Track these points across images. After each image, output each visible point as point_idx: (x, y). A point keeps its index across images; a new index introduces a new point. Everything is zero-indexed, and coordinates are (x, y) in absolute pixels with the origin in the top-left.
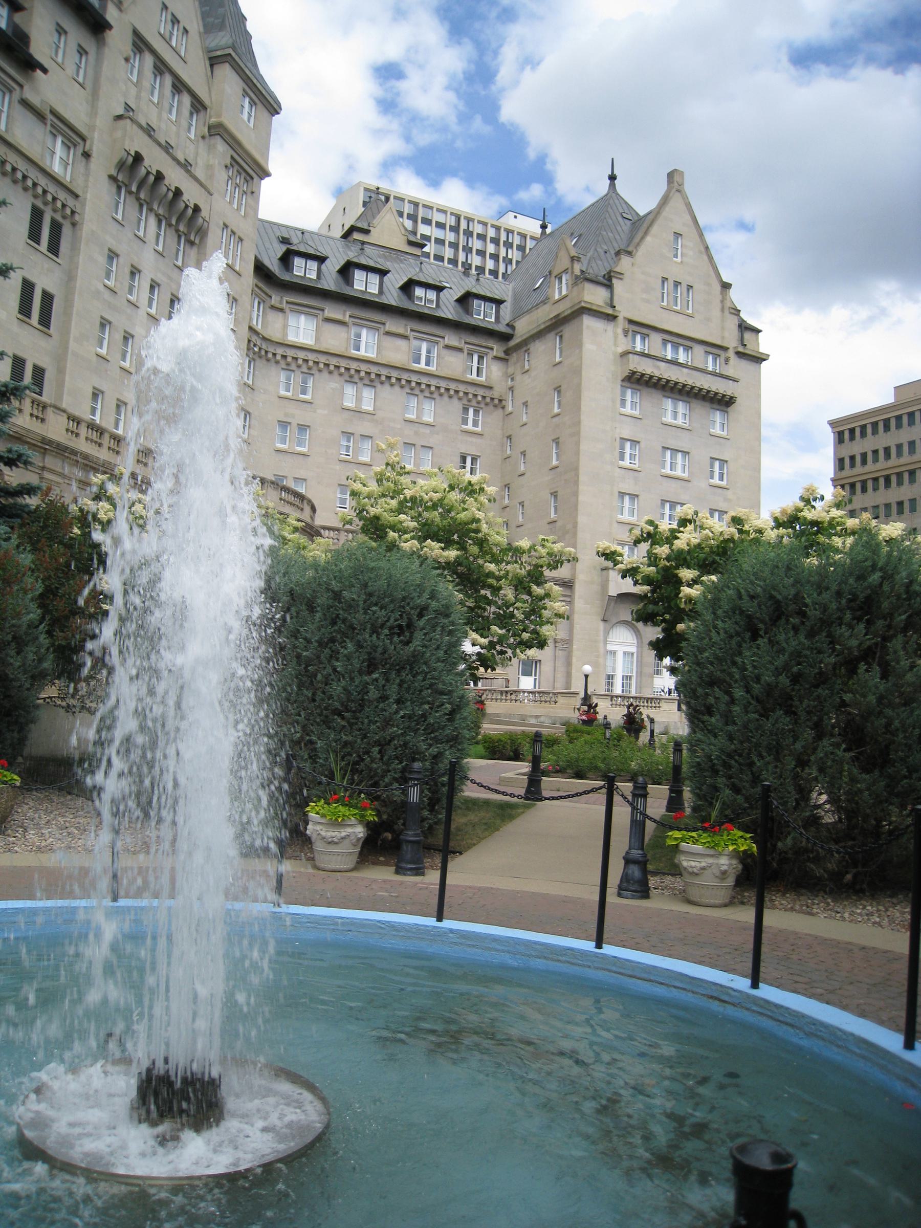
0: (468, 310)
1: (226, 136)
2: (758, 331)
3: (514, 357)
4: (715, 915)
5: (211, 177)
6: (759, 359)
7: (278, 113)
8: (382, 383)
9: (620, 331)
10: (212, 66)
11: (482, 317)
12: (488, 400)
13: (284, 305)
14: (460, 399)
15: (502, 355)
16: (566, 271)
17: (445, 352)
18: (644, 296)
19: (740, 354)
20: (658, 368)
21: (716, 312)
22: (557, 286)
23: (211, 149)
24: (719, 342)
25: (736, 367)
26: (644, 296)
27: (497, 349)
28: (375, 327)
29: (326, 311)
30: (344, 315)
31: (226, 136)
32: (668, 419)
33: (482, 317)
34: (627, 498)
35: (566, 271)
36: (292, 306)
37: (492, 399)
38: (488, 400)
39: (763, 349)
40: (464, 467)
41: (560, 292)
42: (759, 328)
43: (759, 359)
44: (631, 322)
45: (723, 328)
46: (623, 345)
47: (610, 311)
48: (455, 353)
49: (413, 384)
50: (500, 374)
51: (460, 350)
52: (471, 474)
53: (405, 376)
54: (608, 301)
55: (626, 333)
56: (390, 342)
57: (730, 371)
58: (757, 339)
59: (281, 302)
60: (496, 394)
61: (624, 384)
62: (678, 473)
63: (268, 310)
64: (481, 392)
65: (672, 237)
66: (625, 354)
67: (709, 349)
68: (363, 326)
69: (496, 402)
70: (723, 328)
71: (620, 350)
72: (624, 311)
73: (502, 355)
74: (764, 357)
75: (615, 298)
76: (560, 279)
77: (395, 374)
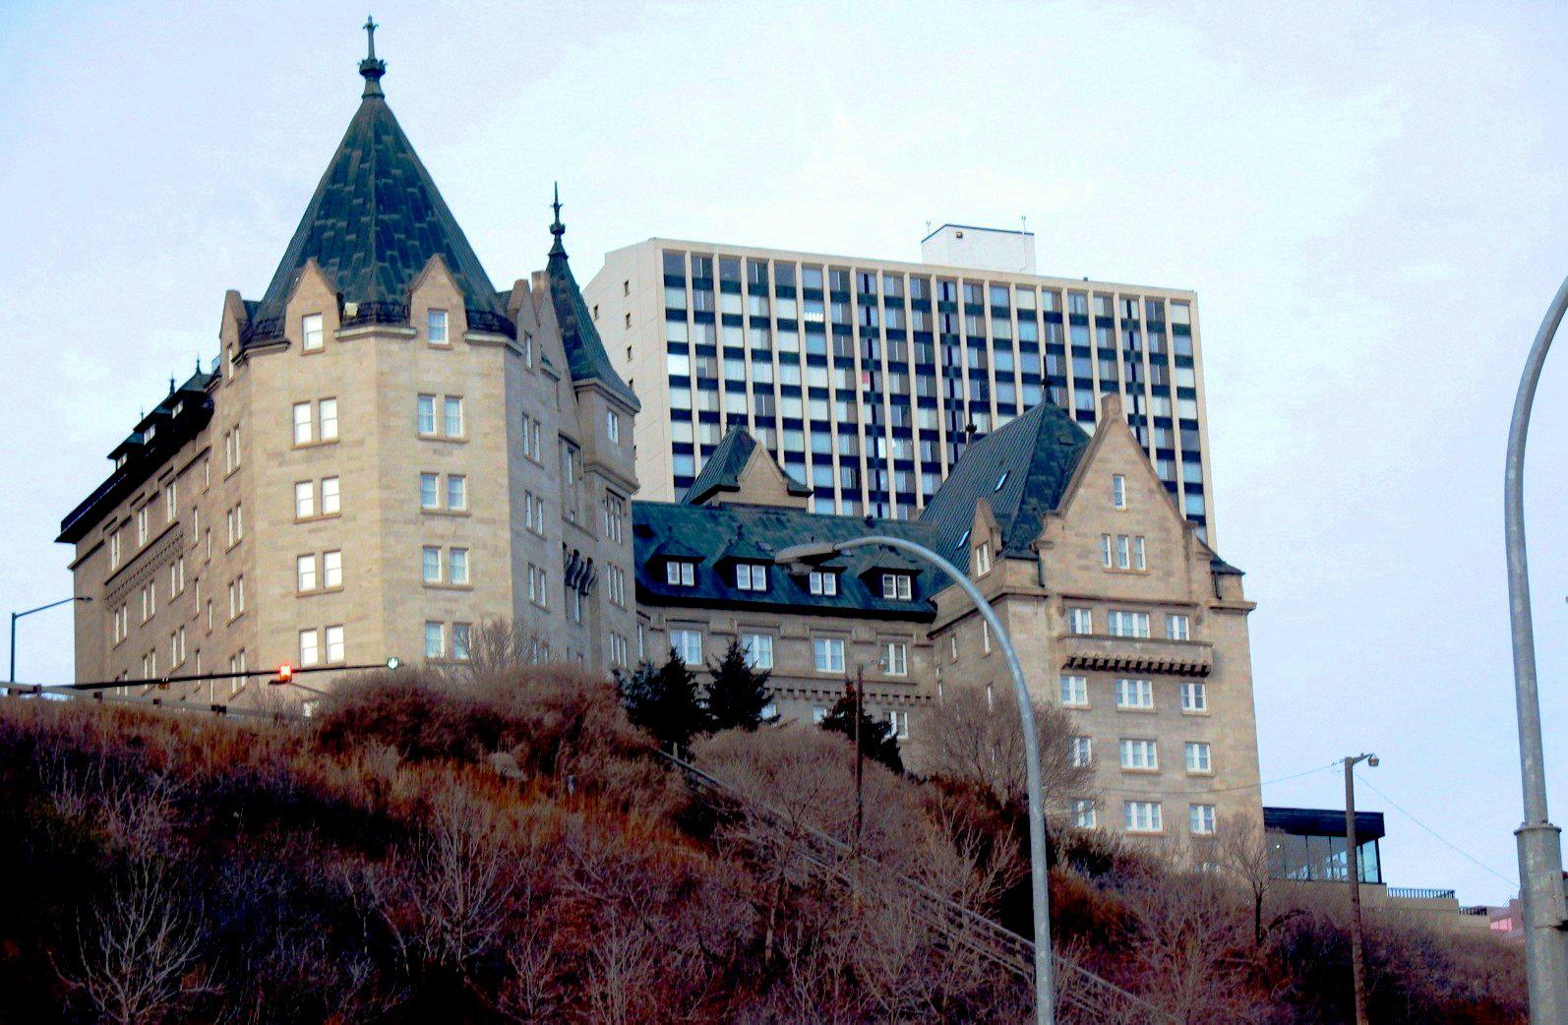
0: (878, 591)
1: (601, 470)
2: (1239, 574)
3: (939, 641)
4: (1045, 979)
5: (592, 518)
6: (1244, 610)
7: (637, 412)
8: (783, 698)
9: (1053, 611)
10: (577, 394)
11: (894, 596)
12: (913, 700)
13: (664, 625)
14: (878, 703)
15: (925, 641)
16: (986, 542)
17: (854, 649)
18: (1081, 562)
19: (1217, 610)
20: (1104, 648)
21: (1178, 562)
22: (978, 555)
23: (589, 486)
24: (1185, 599)
25: (1214, 628)
26: (1081, 562)
27: (918, 631)
28: (835, 635)
29: (711, 624)
30: (732, 625)
31: (601, 470)
32: (1126, 704)
33: (894, 596)
34: (1134, 806)
35: (986, 542)
36: (673, 624)
37: (918, 697)
38: (913, 700)
39: (1248, 597)
40: (326, 528)
41: (983, 569)
42: (1242, 570)
43: (1244, 610)
44: (1065, 597)
45: (1190, 581)
46: (1059, 627)
47: (1039, 591)
48: (866, 648)
49: (820, 694)
50: (924, 665)
51: (872, 643)
52: (452, 549)
53: (809, 686)
54: (1037, 578)
55: (1062, 612)
56: (786, 648)
57: (1205, 634)
58: (1240, 585)
59: (660, 622)
60: (922, 691)
61: (1064, 672)
62: (1144, 765)
63: (649, 633)
64: (903, 691)
65: (1111, 483)
66: (1061, 638)
67: (1113, 606)
68: (754, 633)
69: (923, 700)
70: (1190, 581)
71: (1055, 633)
72: (1054, 586)
73: (925, 641)
74: (1249, 607)
75: (1045, 573)
76: (982, 550)
77: (797, 685)
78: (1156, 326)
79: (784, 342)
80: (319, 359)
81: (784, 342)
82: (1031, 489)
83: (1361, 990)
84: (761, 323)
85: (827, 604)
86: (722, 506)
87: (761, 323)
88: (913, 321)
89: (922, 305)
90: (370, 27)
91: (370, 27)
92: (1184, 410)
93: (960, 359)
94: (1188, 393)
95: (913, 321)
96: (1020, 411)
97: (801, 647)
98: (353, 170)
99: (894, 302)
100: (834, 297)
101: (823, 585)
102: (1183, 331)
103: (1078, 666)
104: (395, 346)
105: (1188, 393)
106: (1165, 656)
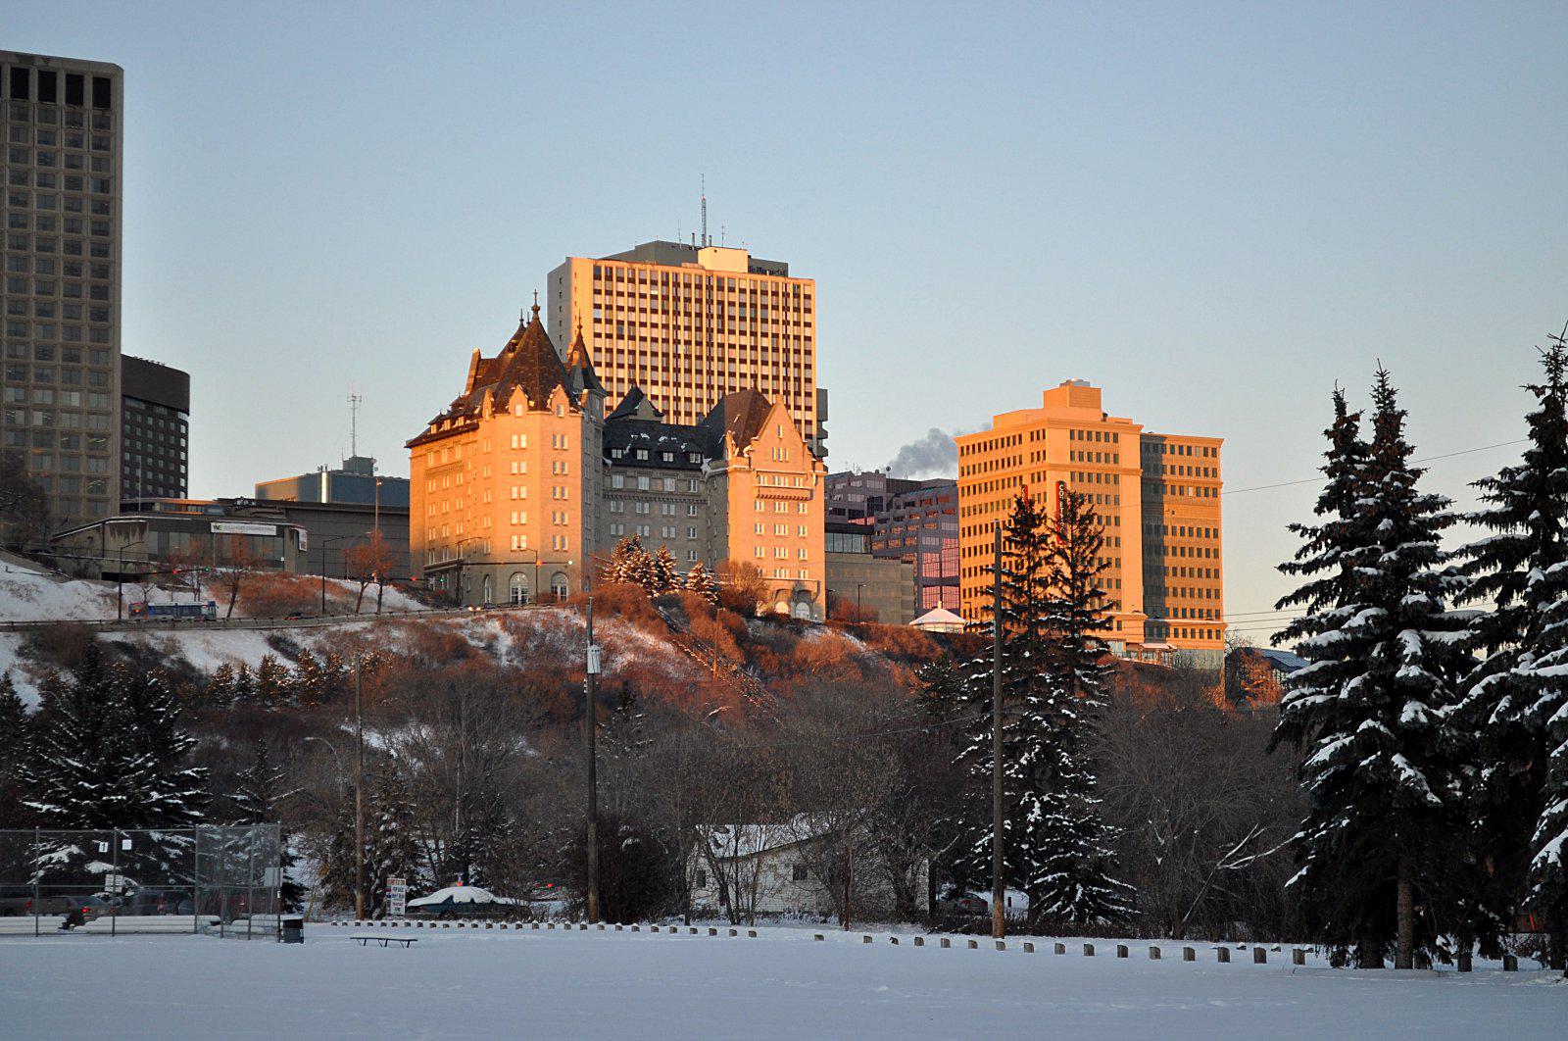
28: (671, 476)
60: (702, 498)
64: (695, 498)
78: (796, 296)
79: (639, 303)
80: (520, 420)
81: (639, 303)
82: (748, 427)
83: (1432, 511)
84: (632, 295)
85: (669, 465)
86: (630, 421)
87: (632, 295)
88: (694, 294)
89: (699, 287)
90: (536, 294)
91: (536, 294)
92: (808, 332)
93: (718, 394)
94: (808, 325)
95: (694, 294)
96: (738, 390)
97: (660, 482)
98: (530, 346)
99: (687, 286)
100: (663, 284)
101: (668, 457)
102: (808, 297)
103: (761, 497)
104: (546, 418)
105: (808, 325)
106: (793, 494)
